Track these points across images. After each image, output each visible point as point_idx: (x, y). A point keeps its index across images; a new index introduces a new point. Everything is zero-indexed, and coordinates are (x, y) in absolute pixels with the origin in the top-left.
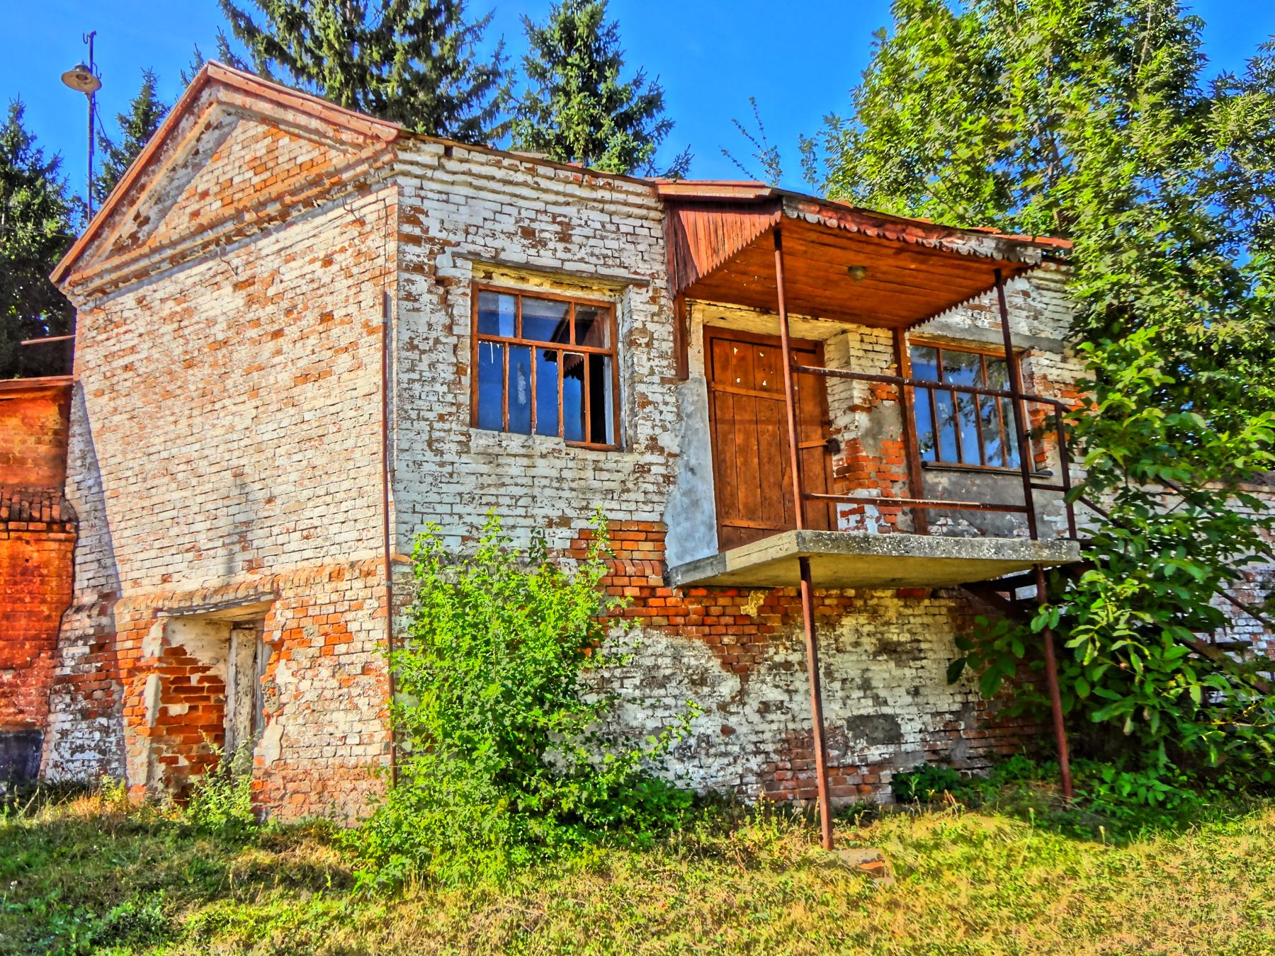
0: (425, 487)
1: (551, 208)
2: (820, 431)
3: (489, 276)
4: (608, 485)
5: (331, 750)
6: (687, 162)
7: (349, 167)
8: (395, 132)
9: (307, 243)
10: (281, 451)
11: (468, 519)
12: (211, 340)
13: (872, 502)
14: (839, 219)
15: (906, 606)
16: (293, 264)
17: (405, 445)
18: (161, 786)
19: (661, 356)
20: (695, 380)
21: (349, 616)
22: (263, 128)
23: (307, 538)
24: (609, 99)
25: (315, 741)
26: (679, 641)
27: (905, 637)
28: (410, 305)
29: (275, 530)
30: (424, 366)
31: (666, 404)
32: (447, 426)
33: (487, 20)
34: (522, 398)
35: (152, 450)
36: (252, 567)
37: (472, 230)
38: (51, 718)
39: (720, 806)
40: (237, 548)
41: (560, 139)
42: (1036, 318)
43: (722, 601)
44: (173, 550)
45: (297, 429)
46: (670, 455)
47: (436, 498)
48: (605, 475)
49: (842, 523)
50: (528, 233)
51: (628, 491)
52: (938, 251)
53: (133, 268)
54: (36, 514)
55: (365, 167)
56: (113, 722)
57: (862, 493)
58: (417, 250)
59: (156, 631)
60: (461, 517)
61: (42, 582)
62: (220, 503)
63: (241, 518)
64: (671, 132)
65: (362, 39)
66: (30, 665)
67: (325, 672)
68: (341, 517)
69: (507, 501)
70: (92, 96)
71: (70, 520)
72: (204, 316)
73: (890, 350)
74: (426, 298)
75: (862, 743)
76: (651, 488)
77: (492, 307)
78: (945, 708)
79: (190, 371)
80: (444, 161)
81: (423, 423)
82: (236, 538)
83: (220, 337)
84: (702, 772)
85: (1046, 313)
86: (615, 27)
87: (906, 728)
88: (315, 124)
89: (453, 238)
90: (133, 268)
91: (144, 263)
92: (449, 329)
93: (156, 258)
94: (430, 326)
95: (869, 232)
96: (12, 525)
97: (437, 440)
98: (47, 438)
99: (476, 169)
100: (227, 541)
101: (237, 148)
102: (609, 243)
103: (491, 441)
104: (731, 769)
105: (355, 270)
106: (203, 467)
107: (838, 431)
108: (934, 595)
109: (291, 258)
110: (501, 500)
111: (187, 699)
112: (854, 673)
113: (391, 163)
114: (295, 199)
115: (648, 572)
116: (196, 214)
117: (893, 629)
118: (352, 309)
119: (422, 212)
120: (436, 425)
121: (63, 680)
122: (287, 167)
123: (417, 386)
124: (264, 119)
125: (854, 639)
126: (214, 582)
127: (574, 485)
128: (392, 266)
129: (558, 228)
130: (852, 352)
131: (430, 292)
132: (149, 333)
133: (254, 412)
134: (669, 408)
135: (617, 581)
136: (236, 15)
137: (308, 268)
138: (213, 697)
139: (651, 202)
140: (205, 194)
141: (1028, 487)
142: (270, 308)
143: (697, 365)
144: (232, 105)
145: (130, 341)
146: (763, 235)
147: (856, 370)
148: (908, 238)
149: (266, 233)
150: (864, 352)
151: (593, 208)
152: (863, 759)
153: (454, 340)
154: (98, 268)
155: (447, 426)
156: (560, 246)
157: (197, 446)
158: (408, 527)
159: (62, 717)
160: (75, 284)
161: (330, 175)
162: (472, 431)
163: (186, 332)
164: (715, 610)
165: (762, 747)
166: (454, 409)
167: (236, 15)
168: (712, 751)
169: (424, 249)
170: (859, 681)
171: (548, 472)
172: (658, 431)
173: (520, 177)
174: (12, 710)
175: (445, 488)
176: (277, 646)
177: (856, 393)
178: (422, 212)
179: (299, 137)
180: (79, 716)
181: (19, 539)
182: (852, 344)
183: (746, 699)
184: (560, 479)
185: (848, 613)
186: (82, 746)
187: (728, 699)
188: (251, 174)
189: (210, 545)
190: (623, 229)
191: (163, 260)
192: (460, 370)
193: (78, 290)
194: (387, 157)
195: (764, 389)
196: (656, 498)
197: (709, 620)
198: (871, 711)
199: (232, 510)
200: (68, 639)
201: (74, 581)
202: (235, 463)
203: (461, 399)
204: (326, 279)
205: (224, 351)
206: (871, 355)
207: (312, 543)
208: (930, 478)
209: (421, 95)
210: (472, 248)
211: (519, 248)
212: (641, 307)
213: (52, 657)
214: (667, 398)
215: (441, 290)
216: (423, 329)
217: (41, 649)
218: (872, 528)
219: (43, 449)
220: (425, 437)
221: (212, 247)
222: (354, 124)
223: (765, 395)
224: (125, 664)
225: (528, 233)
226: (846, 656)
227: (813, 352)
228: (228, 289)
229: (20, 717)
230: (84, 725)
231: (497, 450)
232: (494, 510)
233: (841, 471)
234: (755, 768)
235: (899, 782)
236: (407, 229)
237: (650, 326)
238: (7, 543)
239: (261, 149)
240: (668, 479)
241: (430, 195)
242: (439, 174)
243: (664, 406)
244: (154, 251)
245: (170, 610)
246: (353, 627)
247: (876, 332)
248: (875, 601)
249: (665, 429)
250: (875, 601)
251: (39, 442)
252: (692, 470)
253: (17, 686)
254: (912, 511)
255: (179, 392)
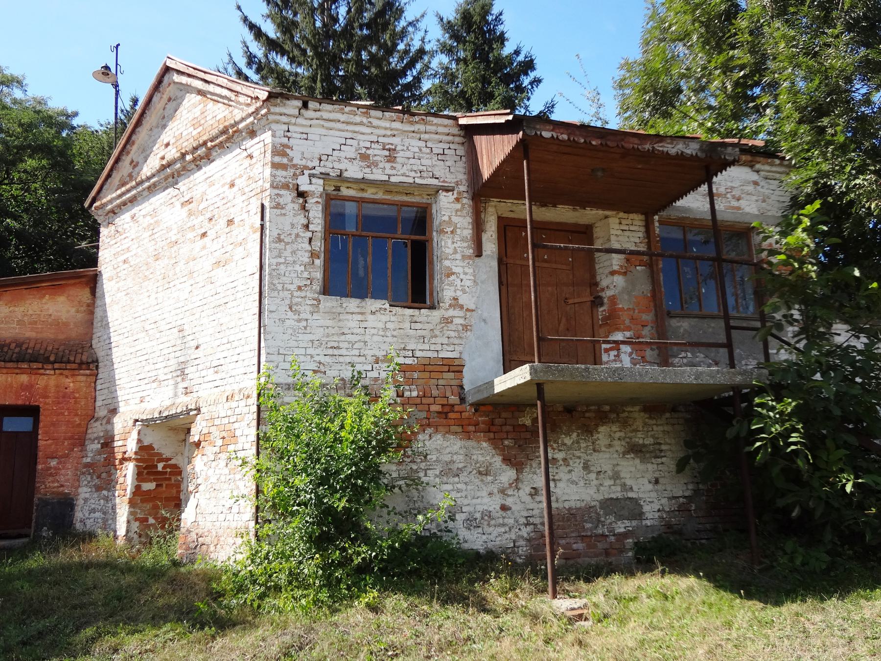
0: (286, 337)
1: (381, 140)
2: (588, 290)
3: (338, 189)
4: (420, 333)
5: (223, 516)
6: (553, 106)
7: (243, 119)
8: (267, 94)
9: (221, 173)
10: (203, 314)
11: (317, 358)
12: (169, 241)
13: (623, 342)
14: (569, 135)
15: (650, 418)
16: (213, 188)
17: (273, 308)
18: (136, 536)
19: (462, 240)
20: (488, 256)
21: (236, 425)
22: (199, 97)
23: (216, 372)
24: (496, 63)
25: (214, 510)
26: (470, 443)
27: (649, 441)
28: (278, 211)
29: (200, 367)
30: (287, 253)
31: (466, 274)
32: (303, 294)
33: (423, 16)
34: (361, 273)
35: (136, 315)
36: (187, 392)
37: (324, 158)
38: (80, 490)
39: (483, 563)
40: (179, 379)
41: (462, 93)
42: (764, 201)
43: (504, 415)
44: (146, 381)
45: (212, 299)
46: (468, 310)
47: (295, 344)
48: (418, 326)
49: (605, 357)
50: (364, 157)
51: (436, 336)
52: (652, 153)
53: (128, 196)
54: (72, 359)
55: (252, 119)
56: (110, 493)
57: (619, 336)
58: (284, 173)
59: (134, 435)
60: (312, 357)
61: (76, 403)
62: (171, 350)
63: (182, 359)
64: (541, 85)
65: (334, 35)
66: (67, 456)
67: (222, 463)
68: (235, 358)
69: (346, 345)
70: (116, 86)
71: (93, 362)
72: (165, 226)
73: (643, 229)
74: (290, 206)
75: (612, 518)
76: (452, 334)
77: (340, 210)
78: (680, 494)
79: (157, 262)
80: (303, 111)
81: (286, 293)
82: (179, 373)
83: (174, 239)
84: (484, 537)
85: (773, 197)
86: (501, 14)
87: (646, 508)
88: (225, 92)
89: (310, 165)
90: (128, 196)
91: (134, 192)
92: (307, 227)
93: (140, 188)
94: (293, 225)
95: (594, 143)
96: (56, 366)
97: (296, 304)
98: (82, 309)
99: (326, 115)
100: (175, 375)
101: (185, 112)
102: (424, 162)
103: (335, 304)
104: (507, 536)
105: (247, 190)
106: (163, 326)
107: (603, 290)
108: (674, 410)
109: (212, 184)
110: (341, 345)
111: (155, 480)
112: (607, 467)
113: (265, 115)
114: (213, 144)
115: (448, 394)
116: (163, 158)
117: (639, 435)
118: (245, 216)
119: (288, 147)
120: (295, 294)
121: (87, 465)
122: (211, 122)
123: (282, 267)
124: (200, 92)
125: (607, 442)
126: (168, 403)
127: (395, 333)
128: (268, 185)
129: (387, 153)
130: (612, 232)
131: (293, 202)
132: (137, 238)
133: (190, 288)
134: (468, 277)
135: (425, 401)
136: (252, 27)
137: (221, 190)
138: (173, 478)
139: (455, 131)
140: (167, 145)
141: (729, 329)
142: (201, 218)
143: (490, 246)
144: (181, 84)
145: (127, 243)
146: (514, 149)
147: (616, 246)
148: (626, 145)
149: (199, 168)
150: (621, 232)
151: (413, 138)
152: (612, 530)
153: (309, 234)
154: (109, 198)
155: (303, 294)
156: (388, 165)
157: (159, 312)
158: (275, 364)
159: (85, 489)
160: (97, 208)
161: (232, 126)
162: (322, 297)
163: (156, 236)
164: (498, 421)
165: (531, 520)
166: (308, 282)
167: (252, 27)
168: (493, 522)
169: (291, 172)
170: (610, 473)
171: (375, 324)
172: (459, 293)
173: (358, 119)
174: (56, 485)
175: (301, 337)
176: (198, 444)
177: (614, 262)
178: (288, 147)
179: (218, 102)
180: (94, 490)
181: (61, 374)
182: (612, 226)
183: (520, 485)
184: (385, 329)
185: (604, 424)
186: (94, 509)
187: (507, 485)
188: (192, 128)
189: (165, 377)
190: (435, 151)
191: (144, 190)
192: (313, 255)
193: (100, 212)
194: (264, 111)
195: (545, 261)
196: (456, 341)
197: (494, 429)
198: (619, 495)
199: (178, 354)
200: (90, 439)
201: (95, 401)
202: (179, 323)
203: (314, 275)
204: (231, 197)
205: (175, 248)
206: (627, 233)
207: (220, 376)
208: (674, 323)
209: (373, 70)
210: (323, 170)
211: (357, 168)
212: (448, 206)
213: (81, 451)
214: (467, 270)
215: (301, 200)
216: (288, 227)
217: (74, 445)
218: (626, 361)
219: (80, 316)
220: (288, 302)
221: (170, 179)
222: (245, 90)
223: (546, 265)
224: (119, 456)
225: (364, 157)
226: (601, 455)
227: (585, 233)
228: (178, 205)
229: (61, 489)
230: (95, 495)
231: (339, 310)
232: (336, 352)
233: (605, 319)
234: (525, 535)
235: (639, 547)
236: (277, 159)
237: (455, 219)
238: (53, 377)
239: (197, 112)
240: (466, 328)
241: (295, 135)
242: (300, 121)
243: (467, 276)
244: (138, 184)
245: (142, 421)
246: (238, 433)
247: (632, 216)
248: (626, 414)
249: (464, 292)
250: (626, 414)
251: (77, 312)
252: (484, 320)
253: (59, 469)
254: (659, 348)
255: (151, 276)
